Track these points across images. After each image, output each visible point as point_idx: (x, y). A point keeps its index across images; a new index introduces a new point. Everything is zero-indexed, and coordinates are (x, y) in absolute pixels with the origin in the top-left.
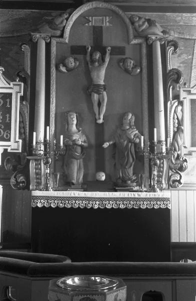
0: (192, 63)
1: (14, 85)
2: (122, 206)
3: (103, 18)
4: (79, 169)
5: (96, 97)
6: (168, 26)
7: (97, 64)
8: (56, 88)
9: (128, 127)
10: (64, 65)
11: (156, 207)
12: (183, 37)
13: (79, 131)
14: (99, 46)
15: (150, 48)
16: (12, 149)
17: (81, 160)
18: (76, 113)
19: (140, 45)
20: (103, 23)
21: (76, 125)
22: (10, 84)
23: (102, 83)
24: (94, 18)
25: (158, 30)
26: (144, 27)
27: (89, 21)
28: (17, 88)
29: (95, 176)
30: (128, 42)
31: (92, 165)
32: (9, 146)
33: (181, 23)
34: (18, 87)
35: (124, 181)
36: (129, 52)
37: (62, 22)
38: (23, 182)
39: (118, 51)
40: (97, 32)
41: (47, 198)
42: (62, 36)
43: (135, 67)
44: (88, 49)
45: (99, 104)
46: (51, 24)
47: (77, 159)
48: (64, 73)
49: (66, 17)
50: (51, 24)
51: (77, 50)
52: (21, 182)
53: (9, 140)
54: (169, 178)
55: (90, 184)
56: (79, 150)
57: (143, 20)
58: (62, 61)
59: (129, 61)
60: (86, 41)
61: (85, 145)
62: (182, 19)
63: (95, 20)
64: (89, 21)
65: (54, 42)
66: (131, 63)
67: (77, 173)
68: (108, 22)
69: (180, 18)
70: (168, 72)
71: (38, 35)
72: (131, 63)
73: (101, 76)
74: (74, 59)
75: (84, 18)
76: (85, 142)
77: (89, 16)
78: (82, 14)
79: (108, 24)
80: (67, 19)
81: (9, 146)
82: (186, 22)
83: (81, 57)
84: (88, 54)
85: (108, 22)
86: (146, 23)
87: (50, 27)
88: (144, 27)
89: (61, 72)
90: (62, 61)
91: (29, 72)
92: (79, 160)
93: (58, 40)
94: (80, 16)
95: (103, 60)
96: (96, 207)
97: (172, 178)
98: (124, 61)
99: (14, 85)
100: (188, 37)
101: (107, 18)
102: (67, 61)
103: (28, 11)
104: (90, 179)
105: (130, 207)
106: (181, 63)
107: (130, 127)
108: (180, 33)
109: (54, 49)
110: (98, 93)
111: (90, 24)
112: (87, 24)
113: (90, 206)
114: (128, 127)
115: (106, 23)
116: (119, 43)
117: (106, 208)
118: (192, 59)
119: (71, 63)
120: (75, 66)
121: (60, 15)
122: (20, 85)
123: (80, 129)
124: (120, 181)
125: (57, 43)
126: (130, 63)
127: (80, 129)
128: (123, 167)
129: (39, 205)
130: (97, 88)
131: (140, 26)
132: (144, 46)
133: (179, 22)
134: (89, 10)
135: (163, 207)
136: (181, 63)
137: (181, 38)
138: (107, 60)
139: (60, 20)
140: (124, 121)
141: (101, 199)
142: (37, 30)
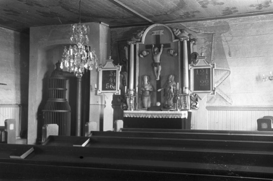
0: (212, 46)
1: (117, 67)
2: (161, 117)
3: (160, 31)
4: (148, 101)
5: (155, 68)
6: (198, 28)
7: (156, 53)
8: (139, 65)
9: (170, 81)
10: (142, 55)
11: (176, 117)
12: (207, 33)
13: (149, 84)
14: (158, 45)
15: (182, 43)
16: (116, 94)
17: (149, 97)
18: (147, 76)
19: (178, 42)
20: (160, 33)
21: (148, 81)
22: (115, 66)
23: (158, 61)
24: (155, 31)
25: (186, 34)
26: (179, 34)
27: (153, 33)
28: (118, 68)
29: (156, 104)
30: (172, 41)
31: (155, 99)
32: (115, 92)
33: (206, 26)
34: (119, 67)
35: (168, 106)
36: (172, 46)
37: (140, 35)
38: (125, 107)
39: (167, 46)
40: (158, 37)
41: (130, 114)
42: (141, 41)
43: (174, 53)
44: (153, 46)
45: (157, 72)
46: (136, 36)
47: (147, 97)
48: (142, 58)
49: (142, 32)
50: (136, 36)
51: (148, 47)
52: (124, 107)
53: (115, 90)
54: (191, 105)
55: (153, 107)
56: (148, 93)
57: (178, 30)
58: (141, 53)
59: (171, 50)
60: (153, 42)
61: (151, 90)
62: (206, 23)
63: (156, 32)
64: (153, 33)
65: (138, 44)
66: (172, 52)
67: (147, 102)
68: (162, 32)
69: (205, 23)
70: (191, 54)
71: (130, 42)
72: (172, 52)
73: (158, 59)
74: (146, 51)
75: (151, 32)
76: (151, 89)
77: (153, 31)
78: (150, 30)
79: (162, 33)
80: (143, 33)
81: (115, 92)
82: (209, 25)
83: (149, 50)
84: (153, 49)
85: (162, 32)
86: (180, 32)
87: (136, 38)
88: (179, 34)
89: (141, 57)
90: (141, 53)
91: (127, 58)
92: (148, 97)
93: (139, 43)
94: (149, 31)
95: (159, 51)
96: (149, 117)
97: (193, 105)
98: (169, 50)
99: (117, 67)
100: (209, 33)
101: (162, 30)
102: (143, 53)
103: (130, 27)
104: (154, 105)
105: (164, 117)
106: (206, 46)
107: (172, 81)
108: (205, 31)
109: (138, 47)
110: (156, 66)
111: (154, 34)
112: (152, 35)
113: (147, 117)
114: (170, 81)
115: (161, 33)
116: (167, 42)
117: (168, 118)
118: (212, 44)
119: (145, 53)
120: (147, 54)
121: (140, 32)
122: (119, 67)
123: (149, 83)
124: (167, 106)
125: (139, 44)
126: (172, 51)
127: (149, 83)
128: (167, 100)
129: (126, 116)
130: (156, 65)
131: (176, 33)
132: (179, 42)
133: (205, 26)
134: (153, 27)
135: (179, 117)
136: (206, 46)
137: (206, 34)
138: (161, 51)
139: (140, 34)
140: (169, 79)
141: (152, 114)
142: (130, 40)
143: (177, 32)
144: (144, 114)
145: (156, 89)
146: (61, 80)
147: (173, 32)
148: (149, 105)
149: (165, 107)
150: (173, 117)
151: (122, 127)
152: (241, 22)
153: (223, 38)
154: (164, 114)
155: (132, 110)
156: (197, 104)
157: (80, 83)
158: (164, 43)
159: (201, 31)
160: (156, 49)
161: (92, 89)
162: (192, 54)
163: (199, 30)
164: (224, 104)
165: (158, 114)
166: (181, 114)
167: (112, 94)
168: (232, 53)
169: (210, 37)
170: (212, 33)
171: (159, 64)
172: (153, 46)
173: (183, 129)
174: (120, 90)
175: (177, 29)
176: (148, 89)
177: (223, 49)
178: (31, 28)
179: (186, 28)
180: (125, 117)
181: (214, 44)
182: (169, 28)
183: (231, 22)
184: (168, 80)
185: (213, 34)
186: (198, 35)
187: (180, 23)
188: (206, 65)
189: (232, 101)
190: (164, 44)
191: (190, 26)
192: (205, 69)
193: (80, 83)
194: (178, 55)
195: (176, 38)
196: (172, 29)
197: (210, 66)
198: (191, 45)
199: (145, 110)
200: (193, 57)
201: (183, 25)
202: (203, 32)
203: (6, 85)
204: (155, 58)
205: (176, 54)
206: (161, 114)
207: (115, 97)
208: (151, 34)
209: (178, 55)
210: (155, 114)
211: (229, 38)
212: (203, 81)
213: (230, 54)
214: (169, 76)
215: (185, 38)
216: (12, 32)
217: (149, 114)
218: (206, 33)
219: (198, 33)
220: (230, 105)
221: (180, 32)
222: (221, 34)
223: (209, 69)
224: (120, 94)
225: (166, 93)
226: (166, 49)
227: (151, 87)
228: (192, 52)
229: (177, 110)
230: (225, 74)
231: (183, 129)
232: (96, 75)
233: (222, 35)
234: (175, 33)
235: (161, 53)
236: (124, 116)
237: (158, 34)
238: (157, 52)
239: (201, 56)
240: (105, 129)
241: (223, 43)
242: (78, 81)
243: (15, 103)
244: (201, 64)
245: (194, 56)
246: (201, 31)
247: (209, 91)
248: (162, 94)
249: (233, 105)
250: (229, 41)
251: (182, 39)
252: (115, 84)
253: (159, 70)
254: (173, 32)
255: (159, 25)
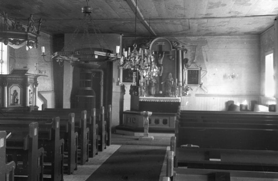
2: (165, 101)
11: (176, 102)
15: (178, 52)
17: (154, 88)
19: (175, 51)
23: (161, 63)
25: (181, 46)
30: (171, 50)
31: (158, 89)
36: (171, 54)
39: (167, 53)
40: (160, 47)
41: (143, 99)
43: (173, 58)
54: (183, 93)
55: (157, 95)
56: (154, 84)
57: (176, 43)
61: (156, 83)
67: (153, 91)
72: (171, 57)
76: (156, 82)
94: (155, 42)
95: (162, 56)
98: (169, 56)
100: (194, 45)
103: (138, 37)
104: (157, 93)
115: (163, 44)
118: (195, 52)
129: (141, 100)
131: (175, 45)
132: (176, 51)
135: (178, 101)
137: (191, 45)
138: (163, 56)
141: (159, 99)
143: (175, 44)
144: (154, 99)
145: (158, 82)
146: (89, 74)
147: (172, 44)
148: (154, 93)
149: (164, 95)
150: (174, 101)
151: (182, 108)
152: (215, 39)
153: (203, 49)
154: (168, 99)
155: (145, 96)
156: (187, 92)
157: (102, 76)
158: (166, 50)
159: (188, 43)
160: (160, 55)
161: (114, 81)
162: (185, 59)
163: (187, 43)
164: (203, 93)
165: (163, 99)
166: (179, 99)
167: (130, 85)
168: (209, 60)
169: (194, 48)
170: (196, 45)
171: (162, 65)
172: (158, 52)
173: (255, 112)
174: (136, 83)
175: (175, 42)
176: (154, 82)
177: (203, 57)
178: (65, 35)
179: (178, 40)
180: (141, 101)
181: (197, 52)
182: (170, 42)
183: (207, 38)
184: (168, 76)
185: (196, 46)
186: (186, 46)
187: (174, 37)
188: (196, 68)
189: (208, 91)
190: (165, 51)
191: (181, 39)
192: (195, 71)
193: (102, 76)
194: (175, 59)
195: (173, 48)
196: (171, 42)
197: (198, 69)
198: (184, 53)
199: (152, 96)
200: (185, 61)
201: (176, 38)
202: (190, 44)
203: (48, 76)
204: (159, 61)
205: (174, 59)
206: (166, 99)
207: (131, 86)
208: (156, 44)
209: (175, 59)
210: (162, 99)
211: (206, 50)
212: (194, 78)
213: (207, 60)
214: (168, 73)
215: (180, 49)
216: (49, 36)
217: (157, 99)
218: (191, 44)
219: (186, 44)
220: (206, 93)
221: (176, 45)
222: (201, 46)
223: (198, 71)
224: (136, 85)
225: (166, 85)
226: (167, 55)
227: (155, 81)
228: (184, 58)
229: (144, 96)
230: (204, 73)
231: (234, 111)
232: (118, 71)
233: (202, 47)
234: (173, 45)
235: (163, 58)
236: (140, 100)
237: (161, 44)
238: (160, 57)
239: (78, 51)
240: (125, 110)
241: (203, 52)
242: (102, 75)
243: (51, 90)
244: (193, 67)
245: (186, 61)
246: (188, 43)
247: (197, 85)
248: (163, 86)
249: (209, 93)
250: (207, 51)
251: (179, 49)
252: (132, 78)
253: (162, 69)
254: (172, 44)
255: (162, 38)
